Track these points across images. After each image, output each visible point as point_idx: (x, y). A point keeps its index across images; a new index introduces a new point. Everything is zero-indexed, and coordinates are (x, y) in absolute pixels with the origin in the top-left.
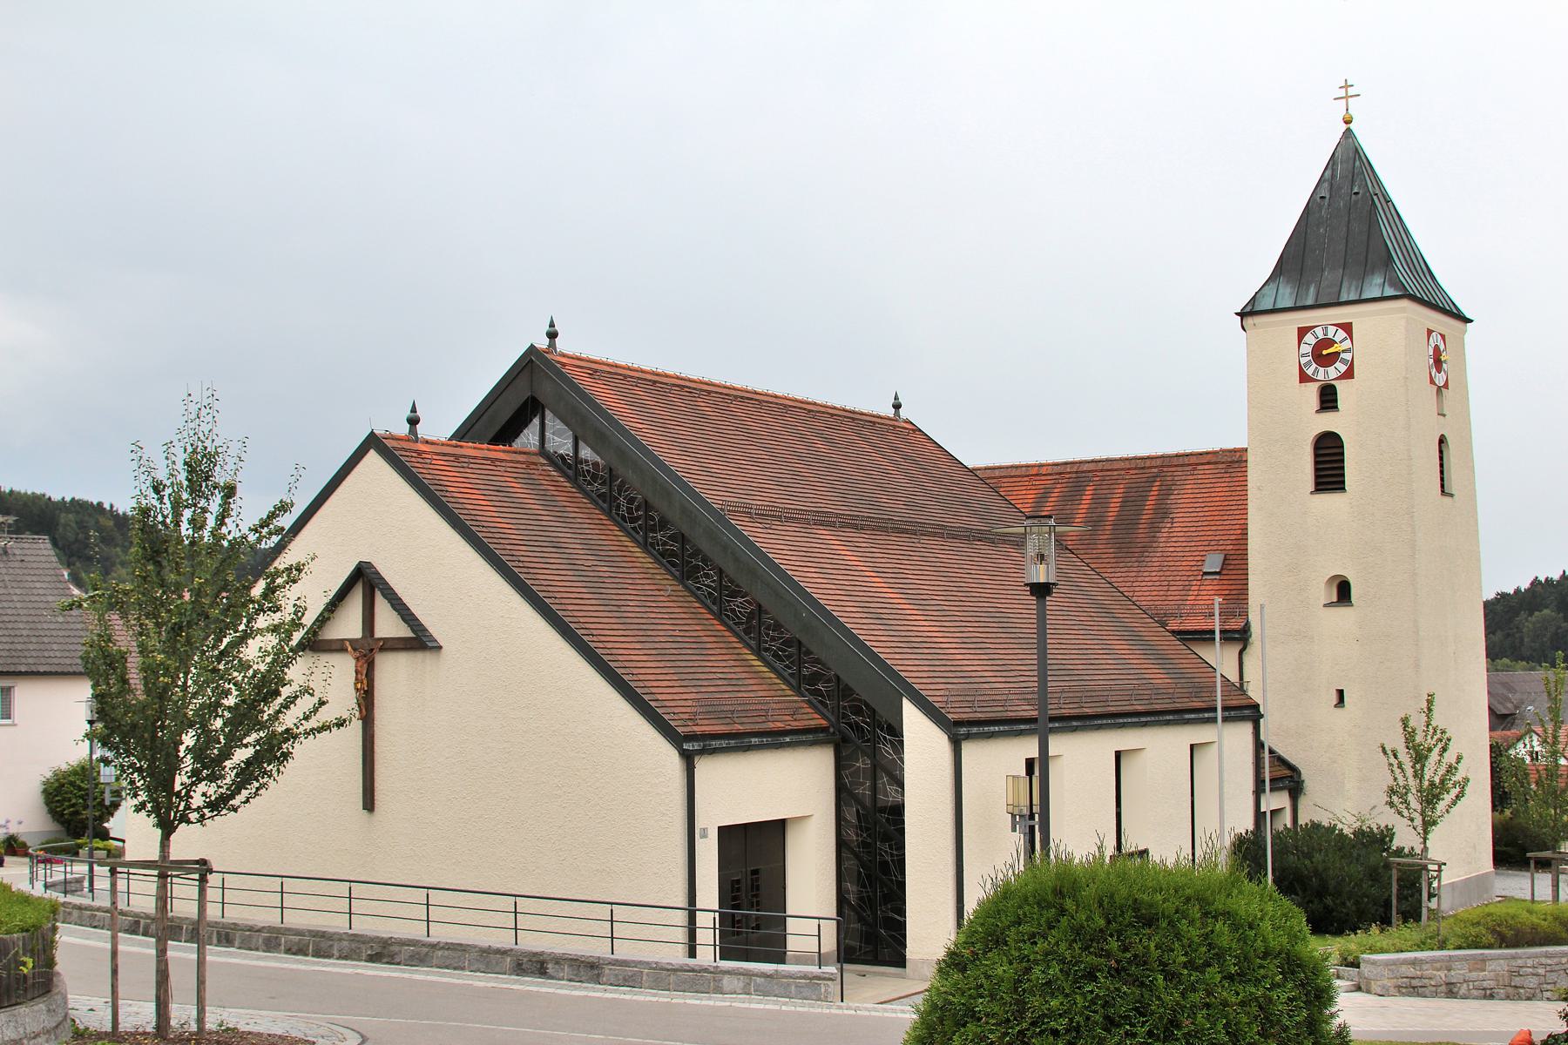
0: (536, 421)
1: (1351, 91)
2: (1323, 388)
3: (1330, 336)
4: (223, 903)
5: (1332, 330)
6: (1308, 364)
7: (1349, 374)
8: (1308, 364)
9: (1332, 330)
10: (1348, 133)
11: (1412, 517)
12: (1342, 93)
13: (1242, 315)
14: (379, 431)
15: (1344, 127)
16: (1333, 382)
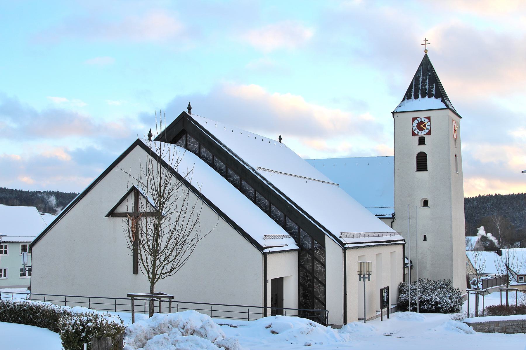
0: (184, 138)
2: (420, 138)
3: (423, 121)
4: (116, 304)
5: (423, 119)
6: (415, 130)
7: (429, 133)
8: (415, 130)
9: (423, 119)
10: (426, 56)
11: (450, 180)
12: (424, 43)
13: (393, 113)
16: (424, 136)
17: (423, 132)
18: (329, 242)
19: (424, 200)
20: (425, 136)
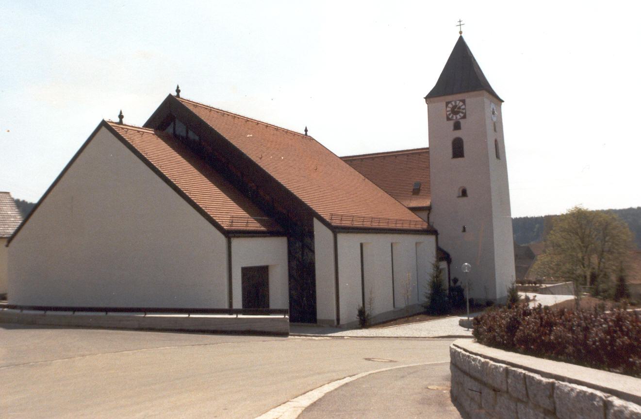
0: (172, 125)
1: (462, 23)
5: (458, 102)
7: (464, 117)
8: (450, 114)
9: (458, 102)
14: (106, 120)
15: (460, 35)
17: (458, 117)
18: (317, 225)
19: (463, 188)
20: (461, 121)
